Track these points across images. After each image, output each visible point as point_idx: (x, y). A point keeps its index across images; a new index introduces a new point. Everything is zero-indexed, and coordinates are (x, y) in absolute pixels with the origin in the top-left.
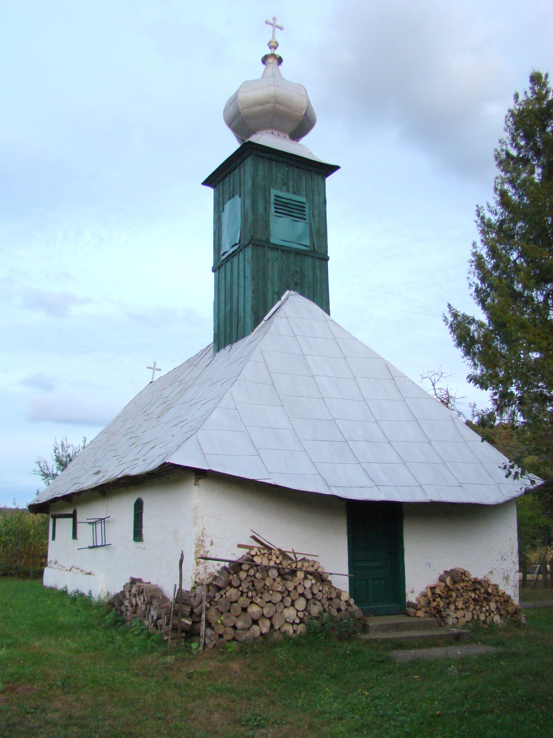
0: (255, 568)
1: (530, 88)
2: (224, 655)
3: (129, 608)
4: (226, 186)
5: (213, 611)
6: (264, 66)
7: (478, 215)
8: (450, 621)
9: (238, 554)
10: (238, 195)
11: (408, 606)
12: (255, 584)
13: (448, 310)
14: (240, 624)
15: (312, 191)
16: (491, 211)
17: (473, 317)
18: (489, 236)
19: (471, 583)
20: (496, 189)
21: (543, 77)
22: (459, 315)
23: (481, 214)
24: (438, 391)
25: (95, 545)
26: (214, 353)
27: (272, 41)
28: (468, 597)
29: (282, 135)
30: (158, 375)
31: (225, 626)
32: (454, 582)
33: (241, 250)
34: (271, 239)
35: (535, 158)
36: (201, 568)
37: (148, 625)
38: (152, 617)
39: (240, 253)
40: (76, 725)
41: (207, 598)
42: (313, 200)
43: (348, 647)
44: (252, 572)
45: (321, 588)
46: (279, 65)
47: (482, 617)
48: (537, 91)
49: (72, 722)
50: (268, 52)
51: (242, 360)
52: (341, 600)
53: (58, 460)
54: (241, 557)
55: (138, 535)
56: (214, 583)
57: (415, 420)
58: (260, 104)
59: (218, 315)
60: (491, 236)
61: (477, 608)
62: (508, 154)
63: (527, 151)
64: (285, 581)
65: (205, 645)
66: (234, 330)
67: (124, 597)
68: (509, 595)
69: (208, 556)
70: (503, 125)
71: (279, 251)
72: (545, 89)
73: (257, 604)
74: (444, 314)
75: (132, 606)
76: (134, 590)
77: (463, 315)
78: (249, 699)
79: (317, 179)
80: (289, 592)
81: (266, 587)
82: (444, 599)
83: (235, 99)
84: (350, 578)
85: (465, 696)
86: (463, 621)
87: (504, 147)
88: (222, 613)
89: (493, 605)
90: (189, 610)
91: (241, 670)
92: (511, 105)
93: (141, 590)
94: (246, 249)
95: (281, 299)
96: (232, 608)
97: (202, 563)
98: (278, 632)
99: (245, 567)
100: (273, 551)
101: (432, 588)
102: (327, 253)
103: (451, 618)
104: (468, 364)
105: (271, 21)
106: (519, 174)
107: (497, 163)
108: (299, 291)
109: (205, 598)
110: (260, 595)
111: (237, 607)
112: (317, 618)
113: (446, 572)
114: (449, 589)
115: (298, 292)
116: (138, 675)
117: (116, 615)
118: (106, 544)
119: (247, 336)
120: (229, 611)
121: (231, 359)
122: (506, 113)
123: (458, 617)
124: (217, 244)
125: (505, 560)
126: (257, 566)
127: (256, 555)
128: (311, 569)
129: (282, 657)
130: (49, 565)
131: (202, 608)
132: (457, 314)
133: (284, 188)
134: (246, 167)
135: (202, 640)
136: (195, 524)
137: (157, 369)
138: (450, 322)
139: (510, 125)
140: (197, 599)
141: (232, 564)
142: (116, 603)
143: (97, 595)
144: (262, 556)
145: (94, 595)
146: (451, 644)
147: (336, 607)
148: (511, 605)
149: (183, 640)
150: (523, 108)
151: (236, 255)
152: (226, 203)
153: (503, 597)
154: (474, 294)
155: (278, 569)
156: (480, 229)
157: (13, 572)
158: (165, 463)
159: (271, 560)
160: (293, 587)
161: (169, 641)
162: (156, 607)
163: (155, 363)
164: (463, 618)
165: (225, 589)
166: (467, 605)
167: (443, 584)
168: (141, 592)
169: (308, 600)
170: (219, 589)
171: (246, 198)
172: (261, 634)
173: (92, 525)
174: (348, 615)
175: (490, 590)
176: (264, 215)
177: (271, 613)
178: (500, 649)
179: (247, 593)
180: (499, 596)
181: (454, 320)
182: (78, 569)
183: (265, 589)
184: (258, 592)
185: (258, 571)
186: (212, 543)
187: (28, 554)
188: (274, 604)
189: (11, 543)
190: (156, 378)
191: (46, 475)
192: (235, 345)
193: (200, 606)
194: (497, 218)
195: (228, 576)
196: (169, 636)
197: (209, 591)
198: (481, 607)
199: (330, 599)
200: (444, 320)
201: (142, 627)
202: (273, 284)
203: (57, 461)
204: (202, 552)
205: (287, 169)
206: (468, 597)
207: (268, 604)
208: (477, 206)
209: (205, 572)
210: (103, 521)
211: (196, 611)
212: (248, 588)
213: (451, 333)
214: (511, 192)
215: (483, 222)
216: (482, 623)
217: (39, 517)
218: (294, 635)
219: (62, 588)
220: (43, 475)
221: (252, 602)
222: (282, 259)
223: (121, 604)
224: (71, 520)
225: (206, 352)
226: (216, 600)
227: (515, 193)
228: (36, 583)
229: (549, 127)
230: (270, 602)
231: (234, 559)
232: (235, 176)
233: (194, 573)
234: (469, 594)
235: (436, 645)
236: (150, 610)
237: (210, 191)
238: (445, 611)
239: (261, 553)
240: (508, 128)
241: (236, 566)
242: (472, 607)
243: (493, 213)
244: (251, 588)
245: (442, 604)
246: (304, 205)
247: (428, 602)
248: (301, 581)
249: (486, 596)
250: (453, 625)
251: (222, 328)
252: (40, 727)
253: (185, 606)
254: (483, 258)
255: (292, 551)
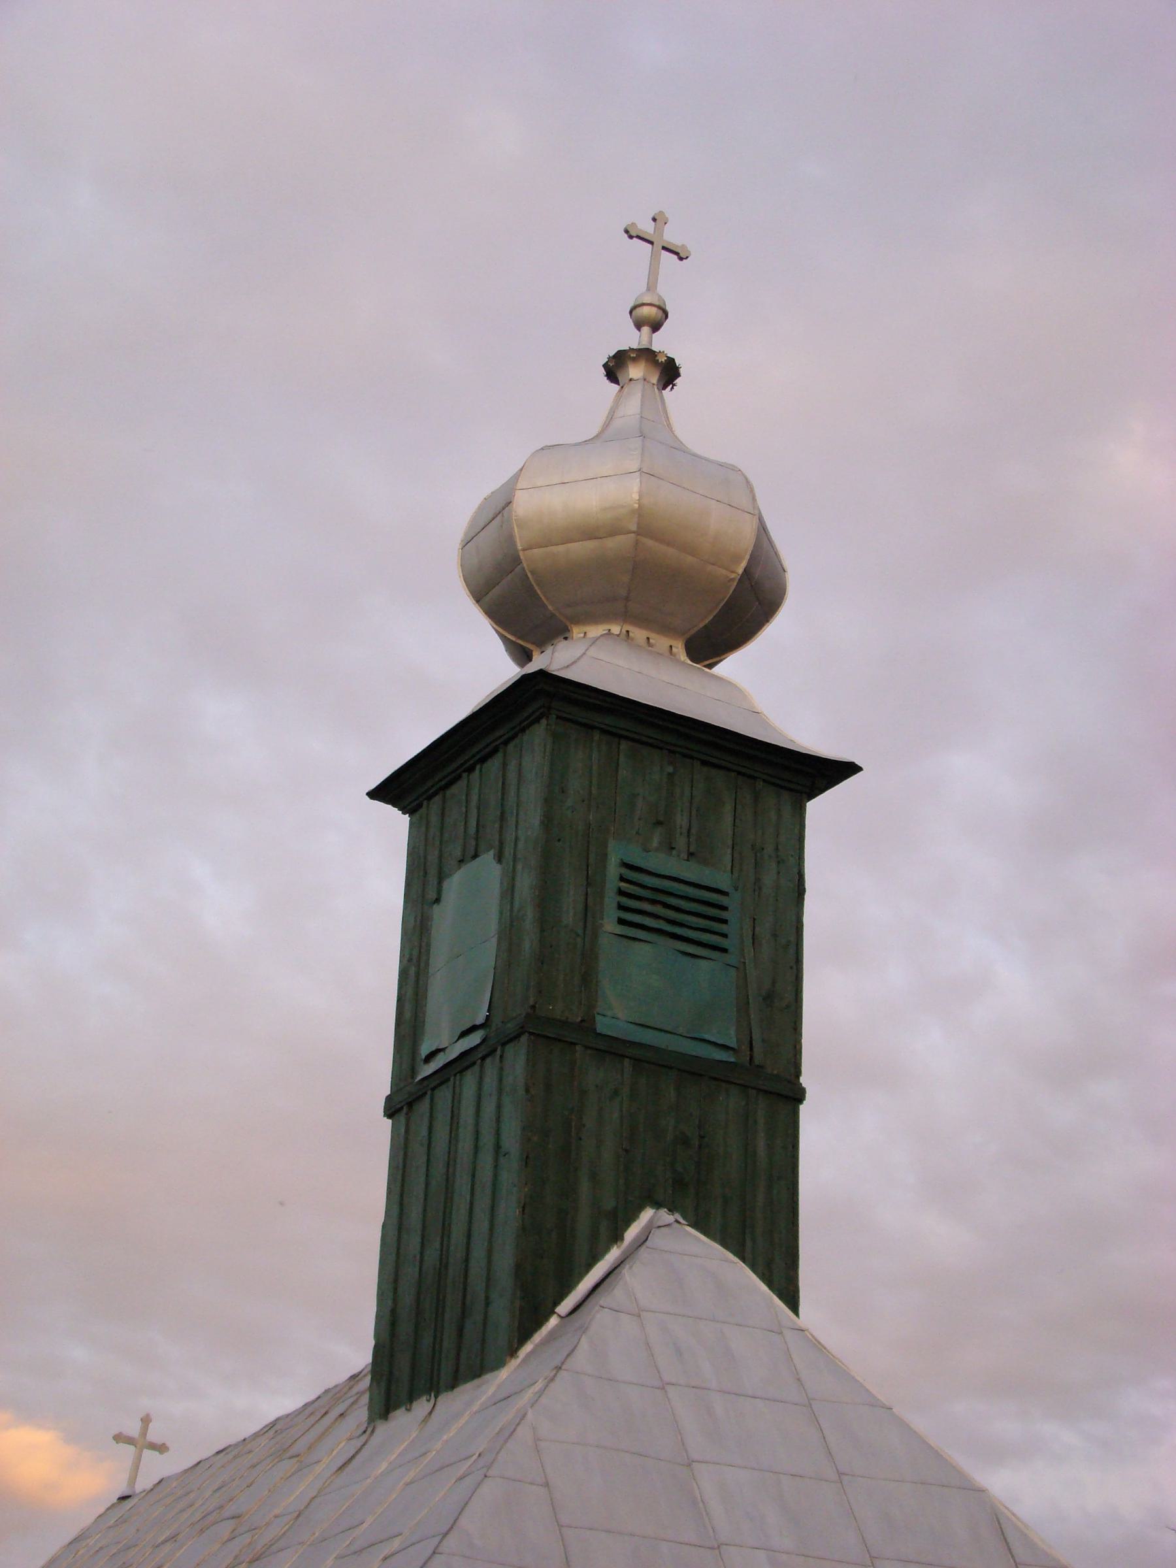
6: (616, 387)
10: (492, 853)
26: (371, 1420)
27: (647, 300)
29: (662, 642)
30: (156, 1468)
33: (492, 1052)
34: (598, 1018)
39: (488, 1061)
42: (758, 880)
50: (632, 339)
51: (463, 1468)
66: (448, 1343)
71: (626, 1062)
94: (510, 1050)
95: (622, 1239)
102: (798, 1073)
105: (648, 228)
115: (684, 1218)
124: (408, 1015)
137: (153, 1447)
151: (474, 1063)
152: (450, 875)
171: (519, 867)
176: (580, 931)
190: (144, 1482)
202: (593, 1177)
205: (670, 769)
225: (341, 1408)
246: (724, 900)
251: (405, 1328)
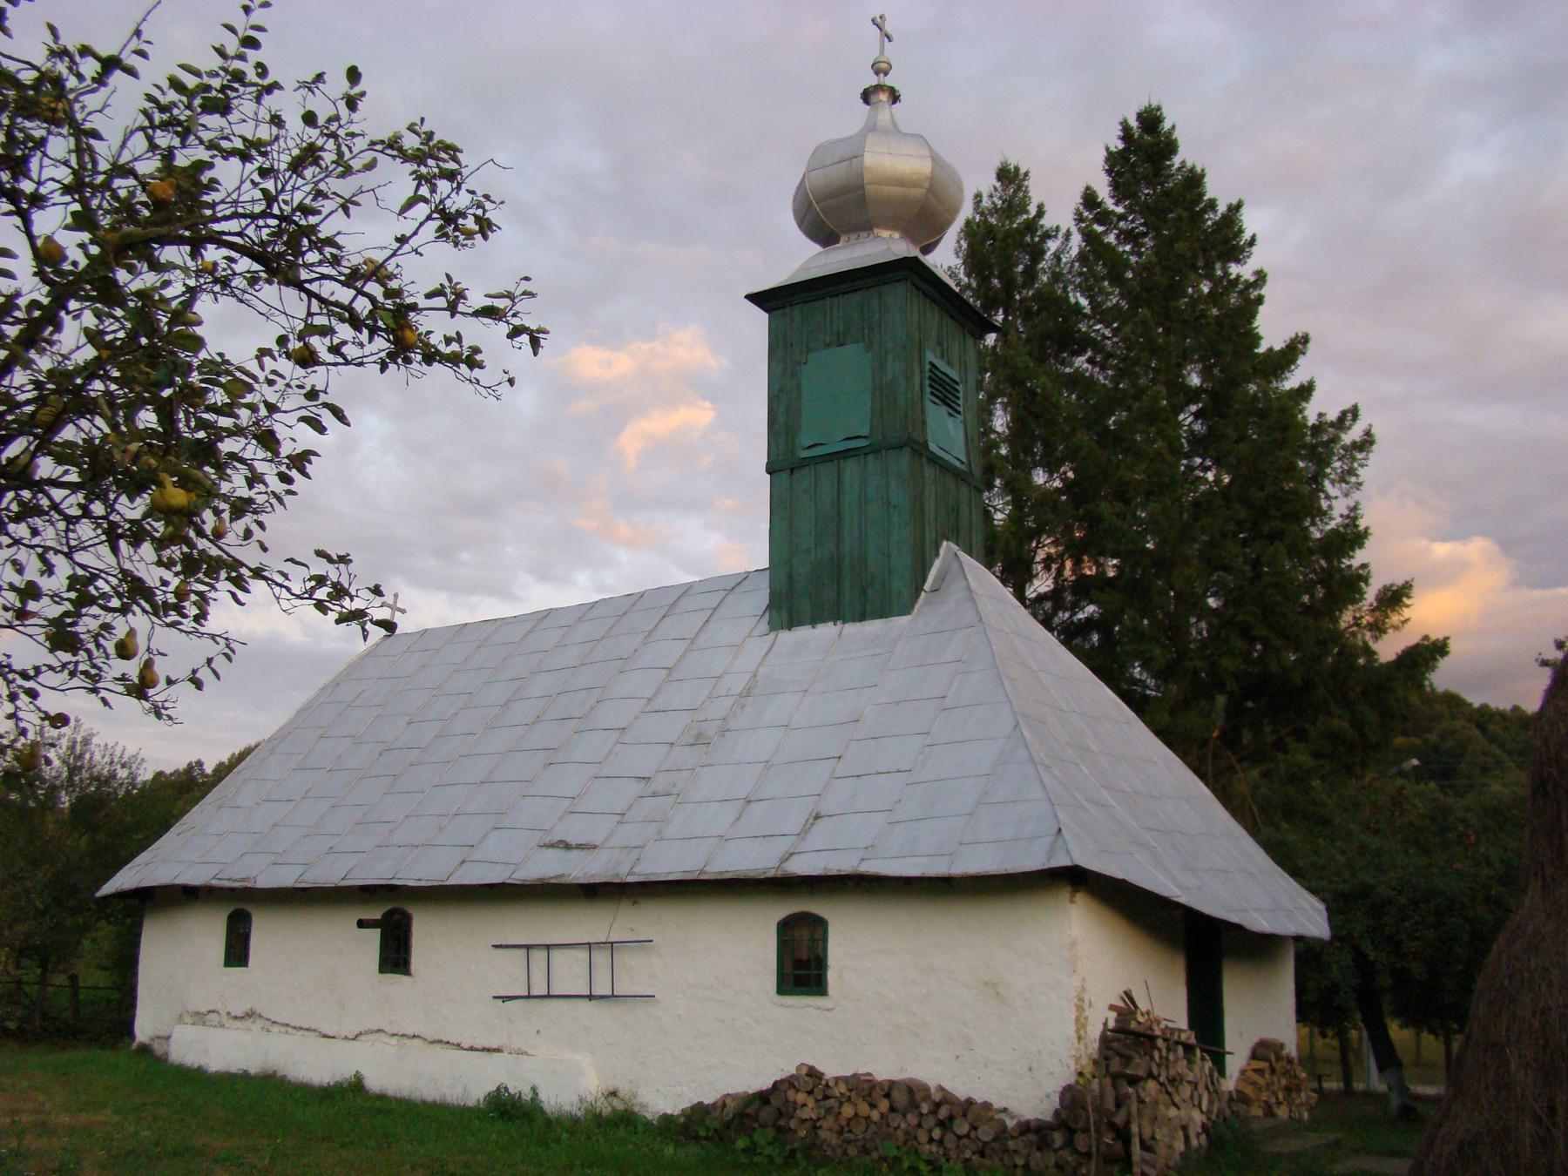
50: (873, 80)
124: (781, 419)
133: (938, 354)
143: (575, 1100)
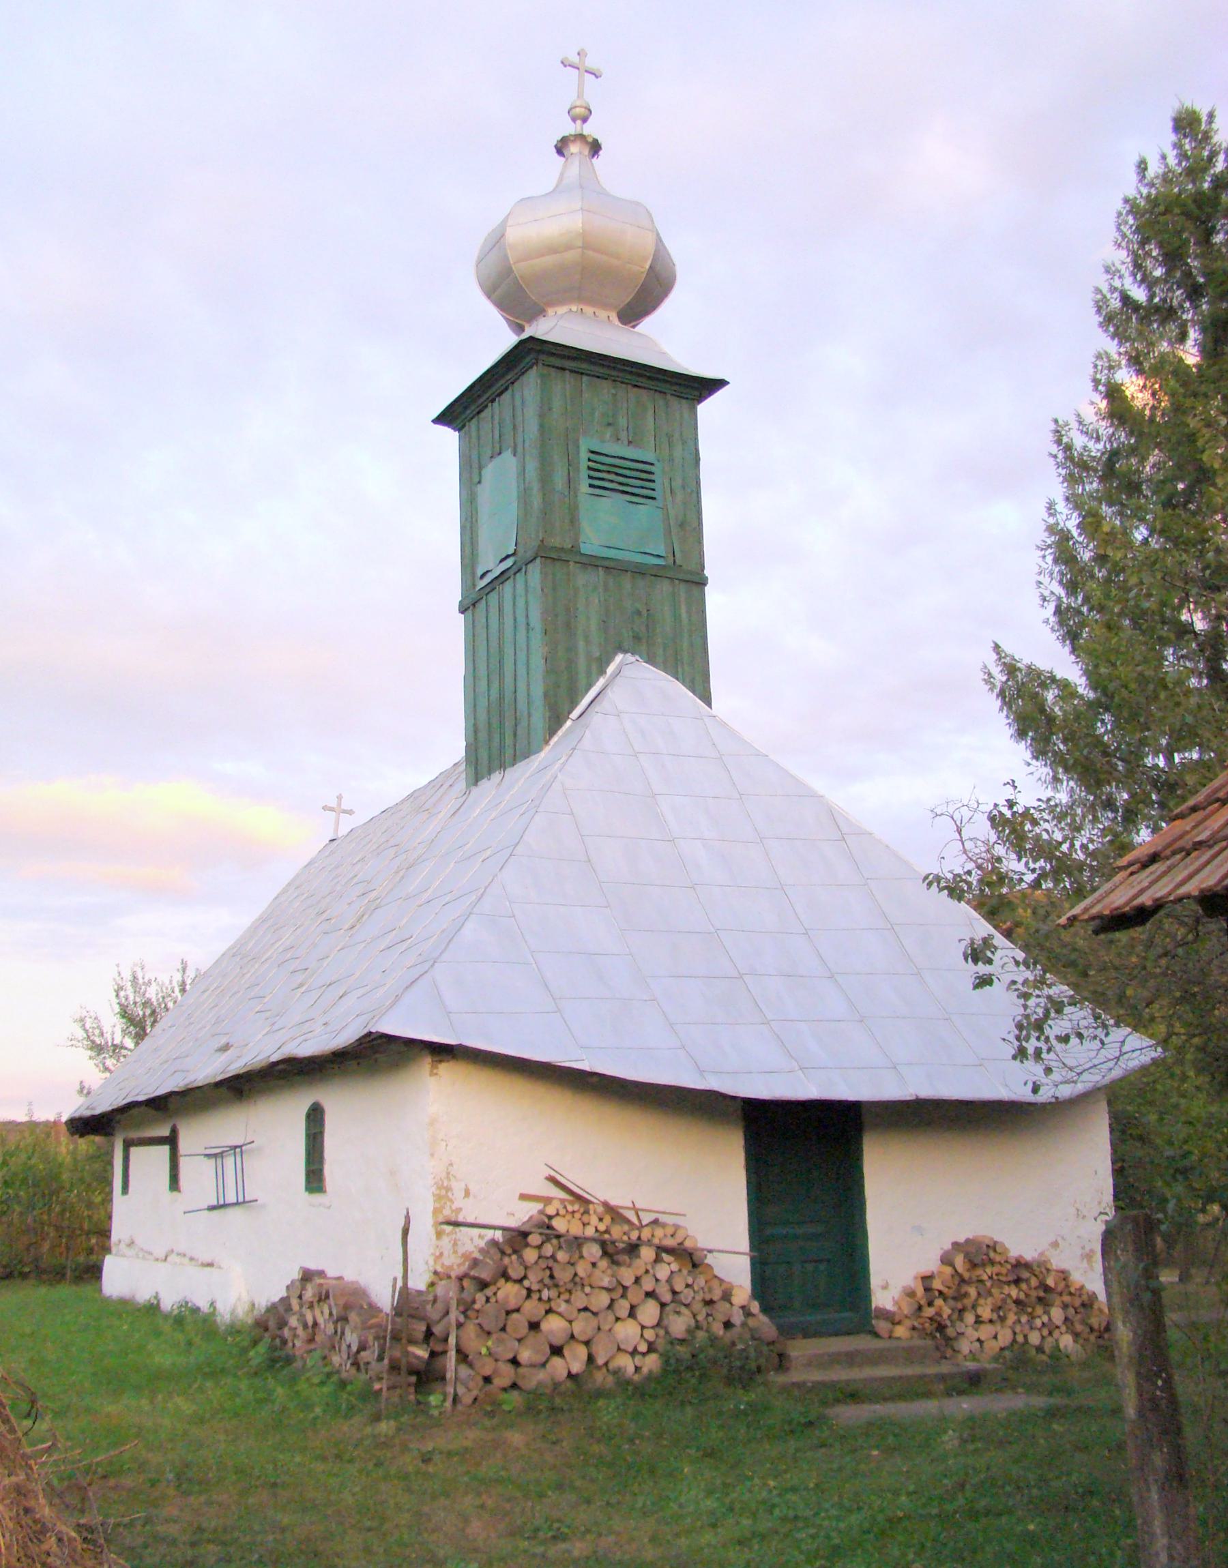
0: (555, 1241)
1: (1175, 146)
2: (494, 1417)
3: (300, 1331)
4: (486, 427)
5: (471, 1329)
6: (562, 160)
7: (1059, 442)
8: (965, 1346)
9: (520, 1214)
11: (877, 1317)
12: (556, 1274)
13: (995, 657)
14: (525, 1355)
15: (670, 437)
16: (1086, 433)
17: (1051, 673)
18: (1084, 489)
19: (1009, 1267)
20: (1096, 382)
21: (1204, 118)
22: (1019, 670)
23: (1065, 440)
24: (968, 845)
25: (221, 1202)
26: (468, 786)
27: (578, 103)
28: (1003, 1296)
31: (496, 1360)
32: (974, 1265)
33: (519, 570)
35: (1187, 305)
36: (446, 1242)
37: (341, 1365)
38: (349, 1346)
40: (213, 1542)
41: (458, 1305)
43: (743, 1399)
44: (548, 1250)
45: (690, 1281)
46: (593, 156)
47: (1034, 1338)
48: (1189, 153)
49: (206, 1536)
50: (570, 129)
52: (732, 1304)
53: (125, 1013)
54: (526, 1219)
55: (315, 1179)
56: (472, 1273)
57: (889, 926)
58: (552, 250)
59: (475, 706)
60: (1087, 488)
61: (1024, 1319)
62: (1126, 299)
63: (1170, 289)
64: (615, 1268)
65: (456, 1400)
66: (509, 741)
67: (289, 1309)
68: (1094, 1293)
69: (460, 1219)
70: (1114, 234)
71: (600, 569)
72: (1208, 148)
73: (560, 1314)
74: (985, 667)
75: (305, 1326)
76: (309, 1294)
77: (1029, 667)
78: (541, 1495)
79: (678, 407)
80: (625, 1288)
81: (577, 1279)
82: (951, 1302)
83: (497, 239)
84: (752, 1259)
85: (962, 1486)
86: (992, 1347)
87: (1117, 283)
88: (489, 1333)
89: (1057, 1314)
90: (424, 1328)
91: (527, 1444)
92: (1130, 186)
93: (324, 1292)
94: (530, 566)
95: (605, 673)
96: (509, 1323)
97: (448, 1234)
98: (604, 1370)
99: (534, 1239)
100: (591, 1206)
101: (926, 1279)
103: (966, 1340)
104: (1040, 779)
105: (575, 59)
106: (1151, 344)
107: (1101, 320)
108: (645, 656)
109: (454, 1304)
110: (565, 1296)
111: (519, 1322)
112: (682, 1341)
113: (956, 1245)
114: (963, 1281)
116: (324, 1459)
117: (272, 1348)
118: (247, 1199)
119: (535, 753)
120: (503, 1329)
121: (503, 804)
122: (1119, 205)
123: (982, 1338)
125: (1084, 1217)
126: (558, 1237)
127: (557, 1214)
128: (670, 1242)
129: (610, 1417)
130: (114, 1250)
131: (449, 1323)
132: (1015, 666)
133: (608, 433)
134: (526, 393)
135: (450, 1390)
136: (432, 1155)
138: (998, 685)
139: (1128, 233)
140: (440, 1306)
141: (508, 1234)
142: (272, 1324)
143: (228, 1309)
144: (569, 1217)
145: (220, 1306)
146: (961, 1393)
147: (721, 1318)
148: (1098, 1312)
149: (412, 1390)
150: (1157, 194)
153: (1080, 1296)
154: (1052, 619)
155: (603, 1244)
156: (1063, 472)
157: (27, 1270)
158: (370, 1033)
159: (588, 1224)
160: (633, 1279)
161: (385, 1393)
162: (356, 1328)
163: (340, 798)
164: (994, 1341)
165: (495, 1284)
166: (1001, 1314)
167: (948, 1270)
168: (323, 1297)
169: (663, 1305)
170: (483, 1285)
172: (570, 1375)
173: (213, 1160)
174: (748, 1336)
175: (1050, 1282)
177: (590, 1332)
178: (1056, 1400)
179: (539, 1291)
180: (1071, 1294)
181: (1008, 680)
182: (184, 1255)
183: (575, 1284)
184: (562, 1290)
185: (560, 1247)
186: (467, 1193)
187: (58, 1228)
188: (595, 1314)
189: (19, 1203)
190: (343, 831)
191: (98, 1049)
192: (512, 773)
193: (446, 1319)
194: (1100, 446)
195: (501, 1259)
196: (384, 1381)
197: (462, 1288)
198: (1032, 1317)
199: (709, 1303)
200: (984, 680)
201: (327, 1369)
202: (588, 641)
203: (123, 1017)
204: (447, 1212)
205: (613, 391)
206: (1003, 1296)
207: (582, 1313)
208: (1056, 421)
209: (455, 1252)
210: (238, 1150)
211: (437, 1330)
212: (541, 1281)
213: (1001, 709)
214: (1132, 385)
215: (1070, 458)
216: (1033, 1352)
217: (86, 1145)
218: (636, 1377)
219: (147, 1297)
220: (91, 1049)
221: (549, 1311)
222: (606, 589)
223: (282, 1324)
224: (165, 1149)
226: (477, 1306)
227: (1144, 386)
228: (87, 1290)
229: (1218, 233)
230: (586, 1309)
231: (513, 1223)
232: (500, 410)
233: (432, 1254)
234: (1006, 1290)
235: (928, 1395)
236: (343, 1333)
237: (449, 438)
238: (953, 1326)
239: (567, 1211)
240: (1123, 239)
241: (518, 1237)
242: (1012, 1318)
243: (1092, 437)
244: (547, 1281)
245: (947, 1311)
247: (916, 1306)
248: (649, 1267)
249: (1042, 1294)
250: (973, 1356)
251: (483, 735)
252: (146, 1546)
253: (414, 1321)
254: (1073, 537)
255: (631, 1205)
